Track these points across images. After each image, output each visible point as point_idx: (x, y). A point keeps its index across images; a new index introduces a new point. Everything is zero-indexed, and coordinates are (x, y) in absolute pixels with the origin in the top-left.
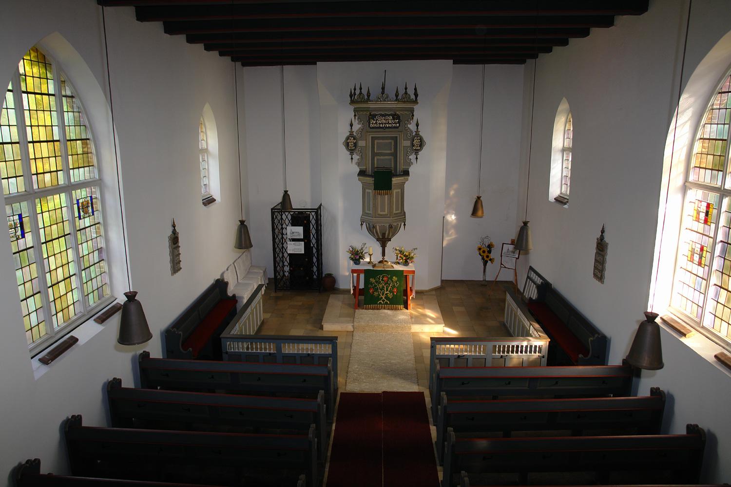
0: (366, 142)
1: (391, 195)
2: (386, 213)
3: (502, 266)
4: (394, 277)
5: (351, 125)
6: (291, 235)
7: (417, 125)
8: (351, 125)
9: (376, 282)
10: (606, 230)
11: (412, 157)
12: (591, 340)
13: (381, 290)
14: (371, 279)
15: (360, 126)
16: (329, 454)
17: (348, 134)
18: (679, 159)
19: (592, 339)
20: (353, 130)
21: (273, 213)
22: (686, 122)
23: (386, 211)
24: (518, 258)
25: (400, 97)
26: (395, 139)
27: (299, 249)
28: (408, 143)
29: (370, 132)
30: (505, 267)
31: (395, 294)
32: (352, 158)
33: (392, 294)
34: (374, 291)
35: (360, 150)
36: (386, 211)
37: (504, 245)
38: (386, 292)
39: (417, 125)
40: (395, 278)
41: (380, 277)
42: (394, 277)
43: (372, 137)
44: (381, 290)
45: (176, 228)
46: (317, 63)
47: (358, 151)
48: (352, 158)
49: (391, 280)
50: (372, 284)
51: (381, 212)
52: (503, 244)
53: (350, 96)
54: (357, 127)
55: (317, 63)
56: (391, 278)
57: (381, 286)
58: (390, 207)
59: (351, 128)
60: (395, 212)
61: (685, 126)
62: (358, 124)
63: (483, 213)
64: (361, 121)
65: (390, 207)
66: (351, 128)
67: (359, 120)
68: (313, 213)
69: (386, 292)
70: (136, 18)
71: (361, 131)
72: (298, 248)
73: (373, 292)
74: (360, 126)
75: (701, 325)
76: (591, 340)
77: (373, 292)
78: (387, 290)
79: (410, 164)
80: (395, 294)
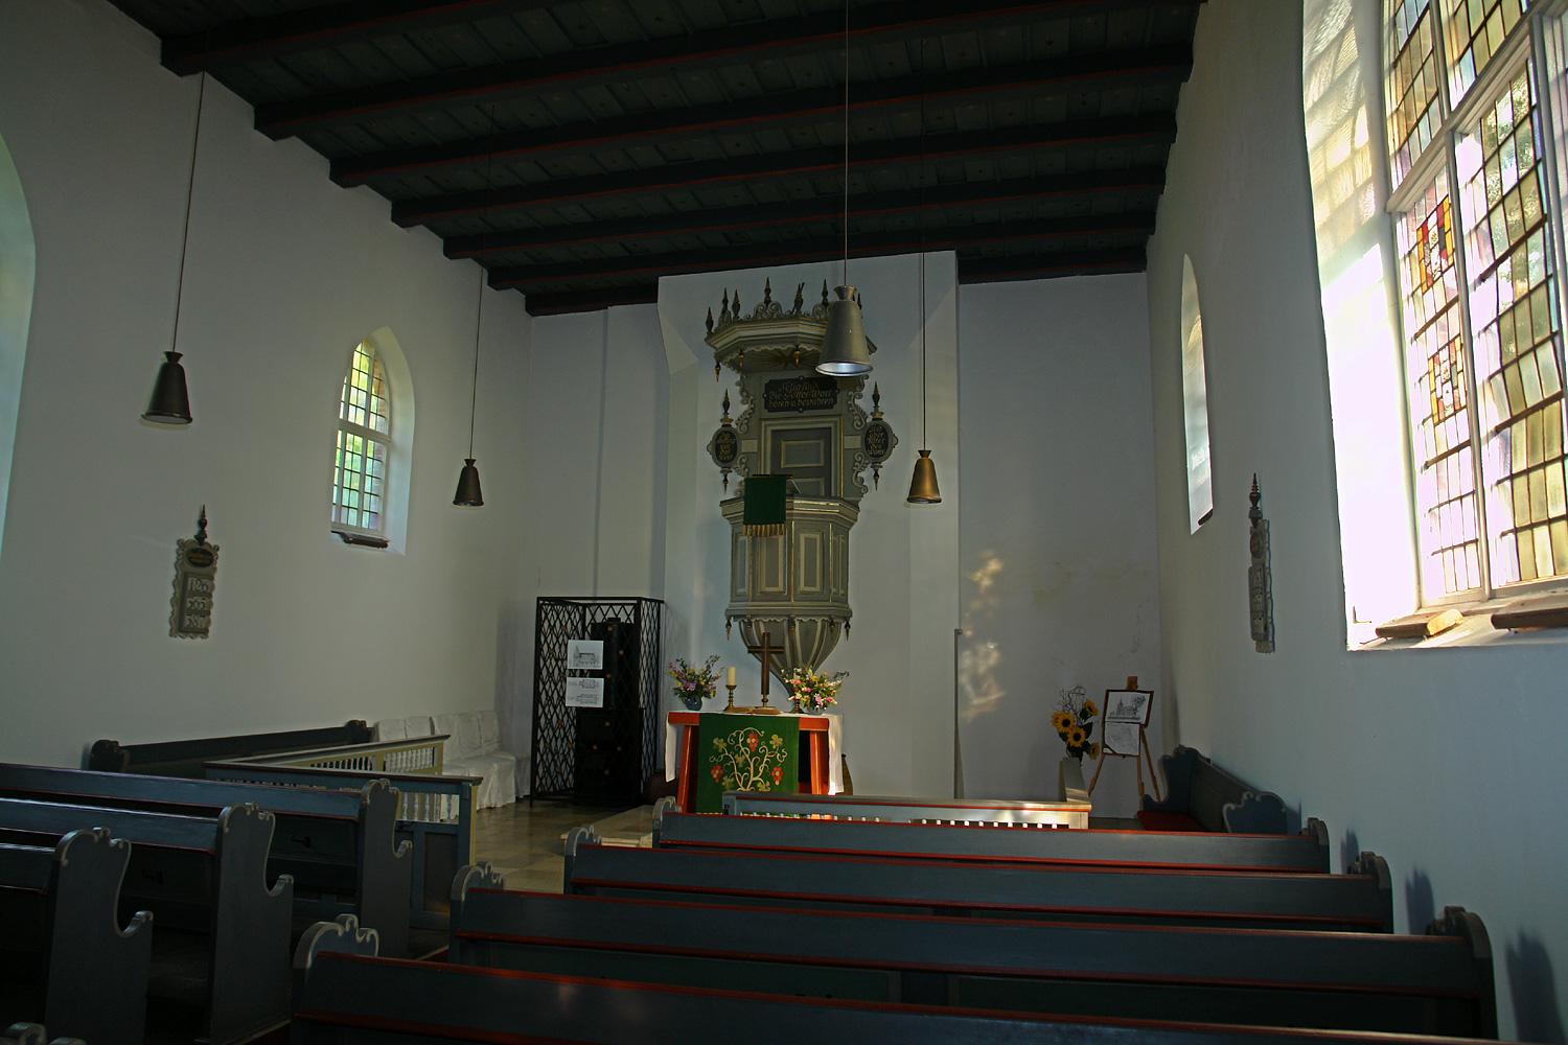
0: (759, 443)
1: (791, 546)
2: (780, 588)
3: (1106, 750)
4: (775, 737)
5: (726, 405)
6: (577, 661)
7: (876, 398)
8: (726, 405)
9: (730, 748)
10: (1263, 490)
11: (866, 474)
12: (1229, 808)
13: (742, 771)
14: (715, 741)
15: (746, 407)
16: (256, 1036)
17: (720, 427)
18: (1352, 142)
19: (1233, 807)
20: (730, 417)
21: (539, 608)
22: (1342, 34)
23: (781, 584)
24: (1146, 725)
25: (806, 308)
26: (826, 434)
27: (591, 696)
28: (855, 442)
29: (768, 419)
30: (1114, 753)
31: (777, 783)
32: (726, 480)
33: (768, 784)
34: (724, 776)
35: (744, 460)
36: (781, 584)
37: (1111, 693)
38: (752, 779)
39: (876, 398)
40: (776, 740)
41: (738, 734)
42: (775, 737)
43: (773, 431)
44: (742, 771)
45: (206, 529)
46: (665, 283)
47: (741, 463)
48: (726, 480)
49: (767, 744)
50: (717, 755)
51: (768, 586)
52: (1108, 691)
53: (707, 322)
54: (738, 409)
55: (665, 283)
56: (768, 738)
57: (740, 760)
58: (791, 573)
59: (726, 413)
60: (802, 587)
61: (1345, 43)
62: (743, 402)
63: (936, 489)
64: (748, 396)
65: (791, 573)
66: (726, 413)
67: (745, 394)
68: (629, 609)
69: (752, 779)
70: (160, 60)
71: (747, 418)
72: (588, 694)
73: (721, 778)
74: (746, 407)
75: (1487, 592)
76: (1229, 808)
77: (721, 778)
78: (756, 773)
79: (861, 490)
80: (777, 783)
